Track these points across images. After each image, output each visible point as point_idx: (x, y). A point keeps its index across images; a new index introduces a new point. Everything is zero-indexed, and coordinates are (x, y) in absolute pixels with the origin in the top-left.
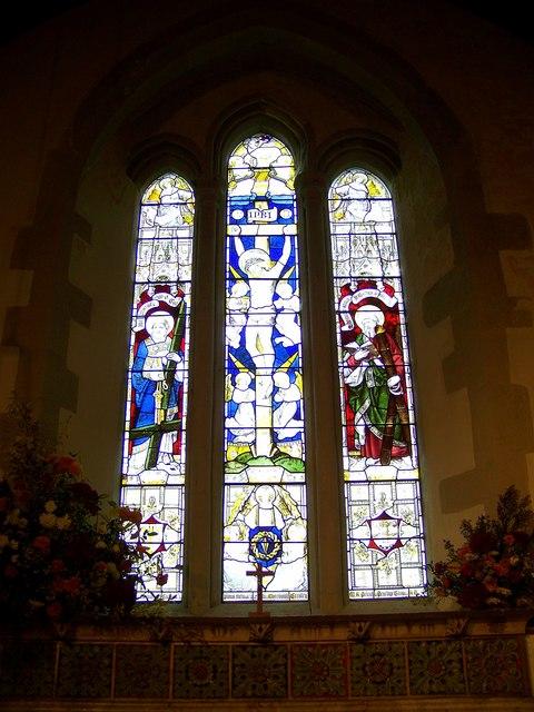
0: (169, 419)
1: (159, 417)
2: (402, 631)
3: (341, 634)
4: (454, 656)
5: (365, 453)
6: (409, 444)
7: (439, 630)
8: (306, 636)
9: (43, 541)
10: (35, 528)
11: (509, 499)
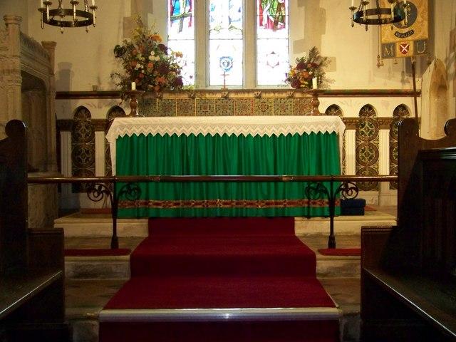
0: (187, 12)
1: (182, 11)
2: (272, 95)
3: (252, 95)
4: (289, 104)
5: (267, 27)
6: (285, 24)
7: (284, 95)
8: (240, 96)
9: (150, 66)
10: (147, 61)
11: (313, 52)
